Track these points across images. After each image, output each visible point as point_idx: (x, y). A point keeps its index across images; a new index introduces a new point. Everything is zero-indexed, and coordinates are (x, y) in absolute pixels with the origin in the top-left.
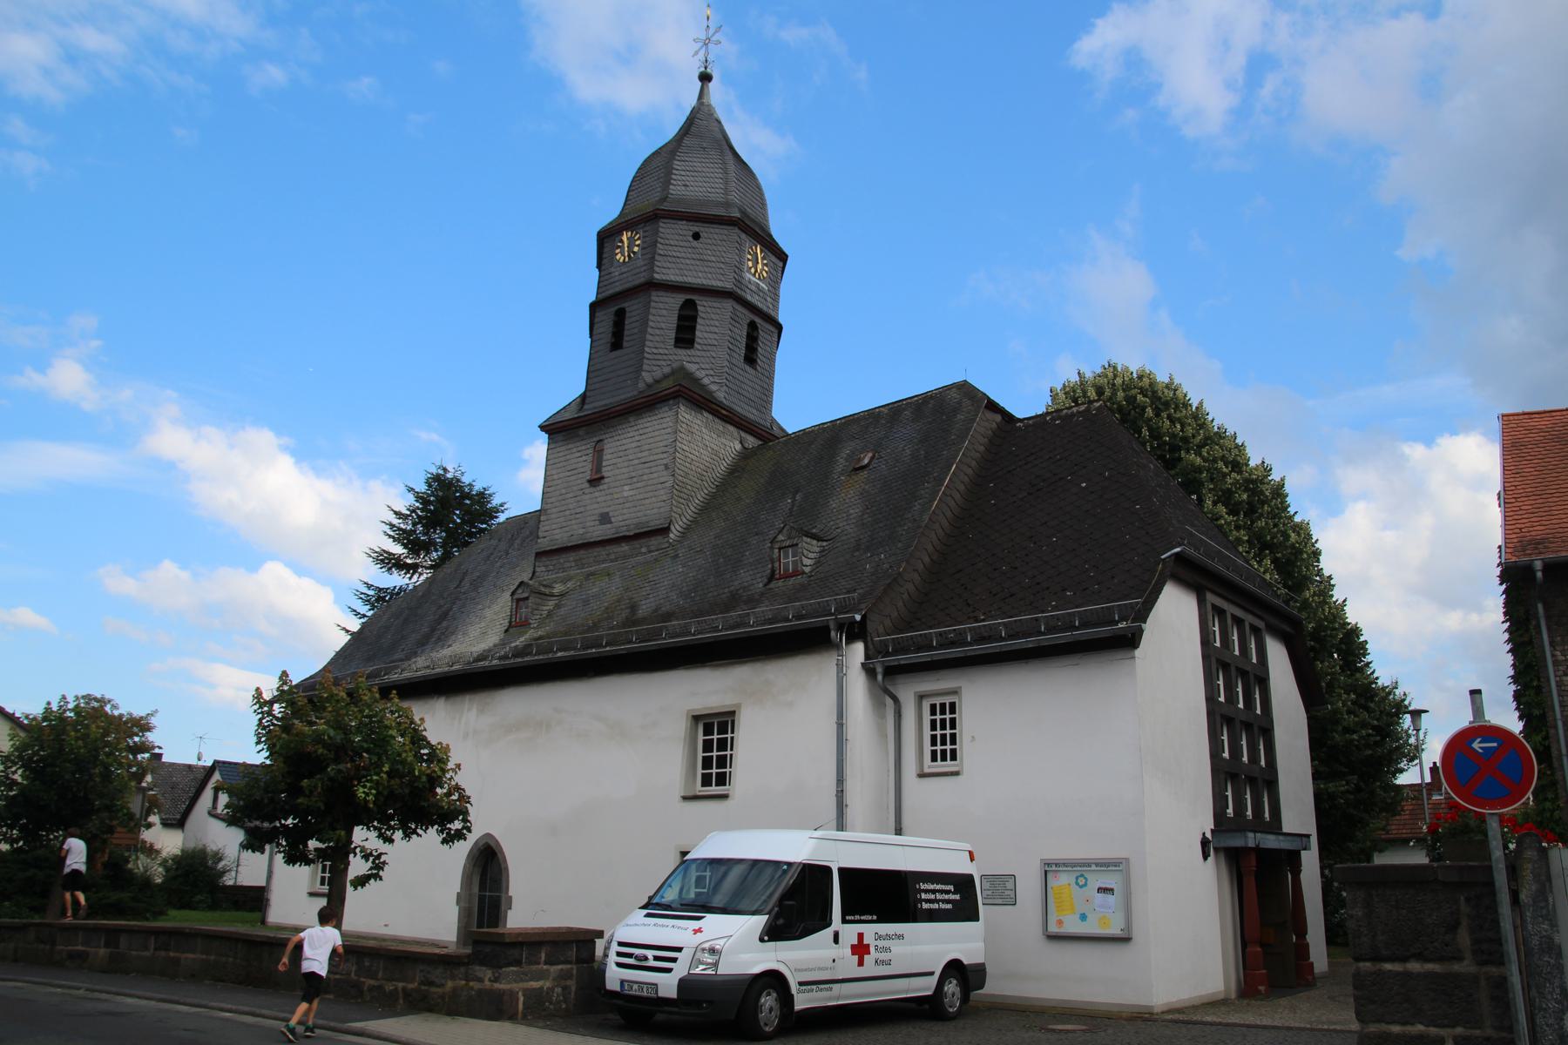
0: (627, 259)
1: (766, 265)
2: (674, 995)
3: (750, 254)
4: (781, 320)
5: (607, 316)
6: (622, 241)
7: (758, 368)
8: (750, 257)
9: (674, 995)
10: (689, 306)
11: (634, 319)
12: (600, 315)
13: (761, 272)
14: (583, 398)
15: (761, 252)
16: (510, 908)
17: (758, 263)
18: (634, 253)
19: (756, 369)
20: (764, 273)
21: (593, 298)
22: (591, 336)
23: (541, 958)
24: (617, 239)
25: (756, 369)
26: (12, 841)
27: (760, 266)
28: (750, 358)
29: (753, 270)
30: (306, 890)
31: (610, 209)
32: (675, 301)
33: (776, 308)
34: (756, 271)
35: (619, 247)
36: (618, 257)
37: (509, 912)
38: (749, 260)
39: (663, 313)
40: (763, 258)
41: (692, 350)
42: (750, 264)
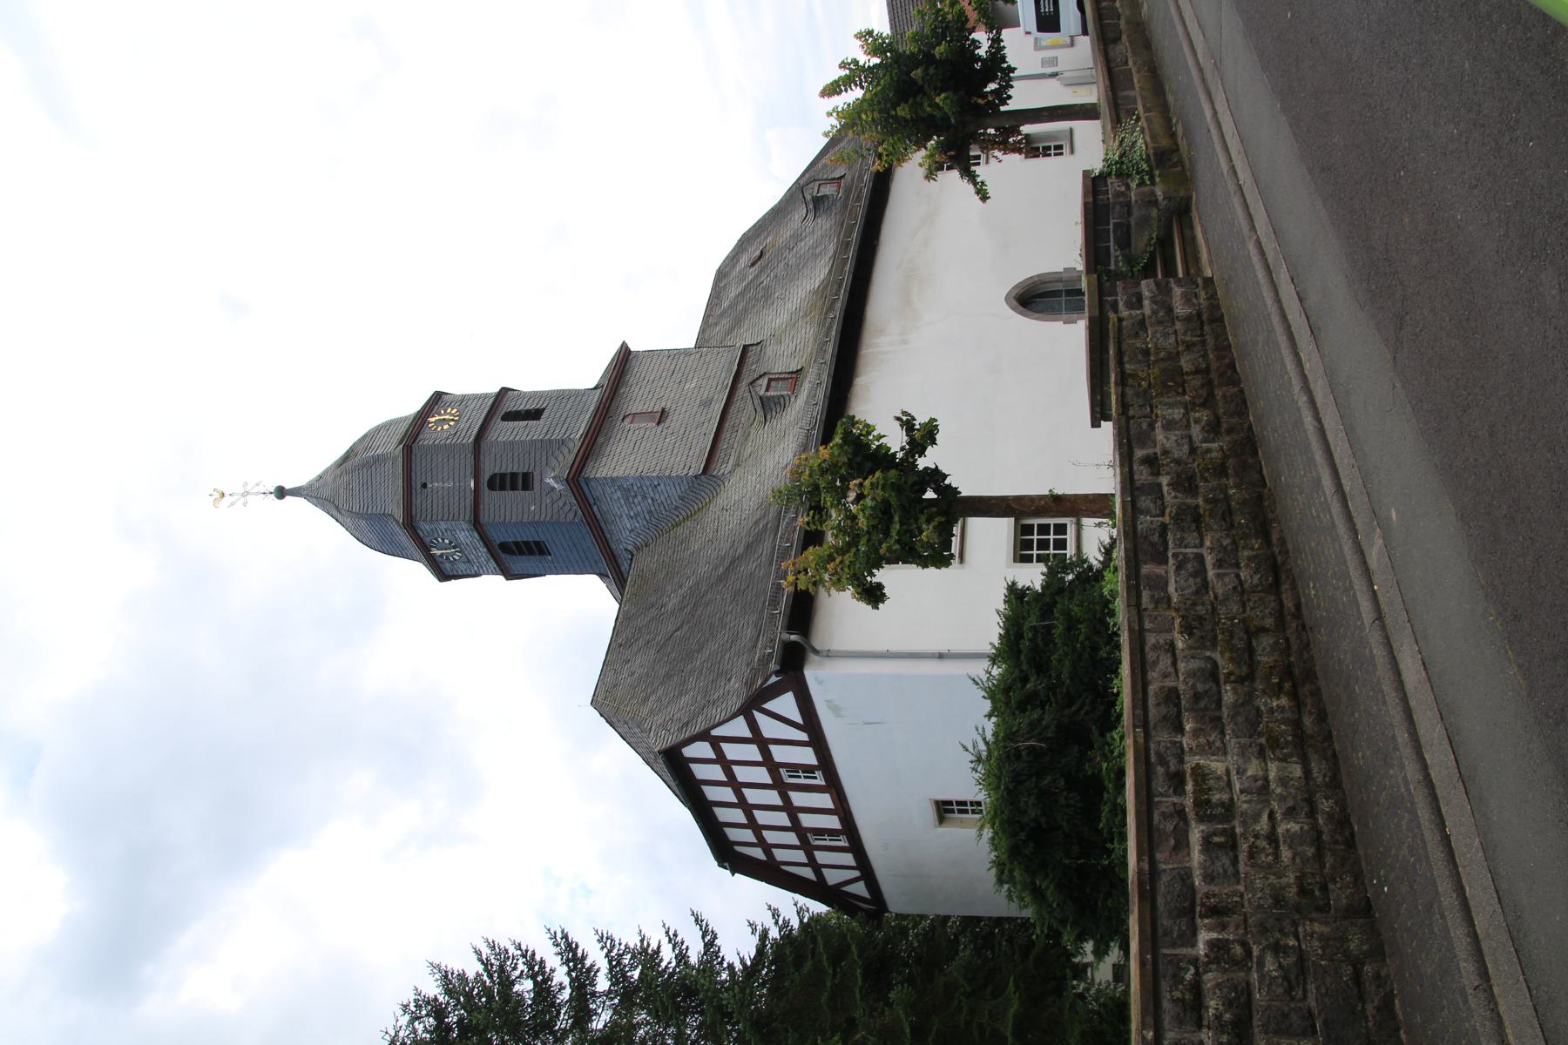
0: (457, 549)
1: (445, 411)
2: (1013, 519)
3: (437, 428)
4: (497, 390)
5: (517, 563)
6: (442, 555)
7: (544, 406)
8: (439, 429)
9: (1013, 519)
10: (492, 485)
11: (528, 533)
12: (515, 570)
13: (453, 415)
14: (602, 575)
15: (433, 416)
16: (1064, 323)
17: (444, 419)
18: (450, 542)
19: (544, 409)
20: (453, 412)
21: (501, 578)
22: (544, 575)
23: (1322, 819)
24: (440, 559)
25: (544, 409)
26: (1071, 557)
27: (447, 417)
28: (535, 414)
29: (452, 423)
30: (1071, 157)
31: (415, 572)
32: (491, 499)
33: (486, 396)
34: (453, 420)
35: (447, 558)
36: (457, 558)
37: (1062, 322)
38: (442, 429)
39: (505, 509)
40: (440, 414)
41: (535, 474)
42: (446, 427)
